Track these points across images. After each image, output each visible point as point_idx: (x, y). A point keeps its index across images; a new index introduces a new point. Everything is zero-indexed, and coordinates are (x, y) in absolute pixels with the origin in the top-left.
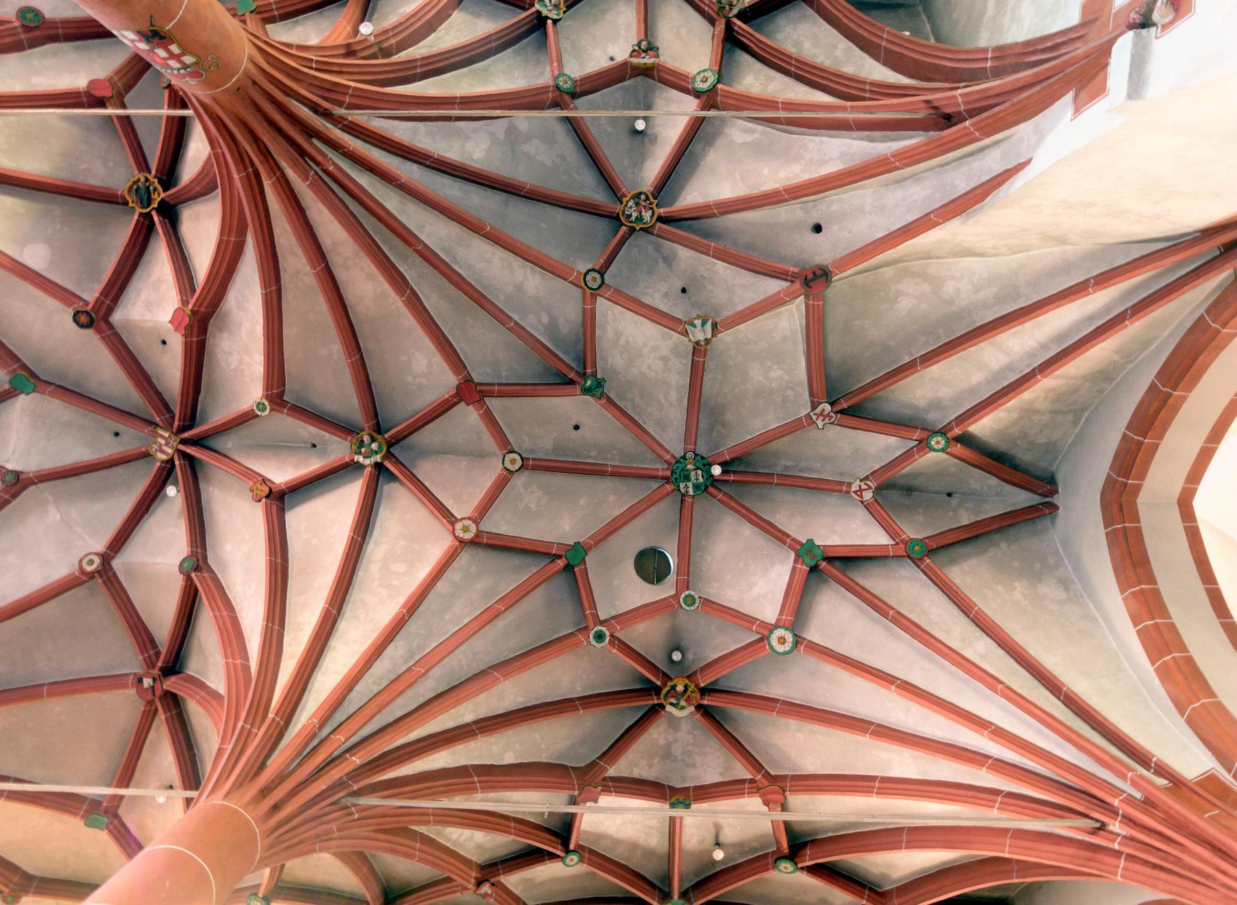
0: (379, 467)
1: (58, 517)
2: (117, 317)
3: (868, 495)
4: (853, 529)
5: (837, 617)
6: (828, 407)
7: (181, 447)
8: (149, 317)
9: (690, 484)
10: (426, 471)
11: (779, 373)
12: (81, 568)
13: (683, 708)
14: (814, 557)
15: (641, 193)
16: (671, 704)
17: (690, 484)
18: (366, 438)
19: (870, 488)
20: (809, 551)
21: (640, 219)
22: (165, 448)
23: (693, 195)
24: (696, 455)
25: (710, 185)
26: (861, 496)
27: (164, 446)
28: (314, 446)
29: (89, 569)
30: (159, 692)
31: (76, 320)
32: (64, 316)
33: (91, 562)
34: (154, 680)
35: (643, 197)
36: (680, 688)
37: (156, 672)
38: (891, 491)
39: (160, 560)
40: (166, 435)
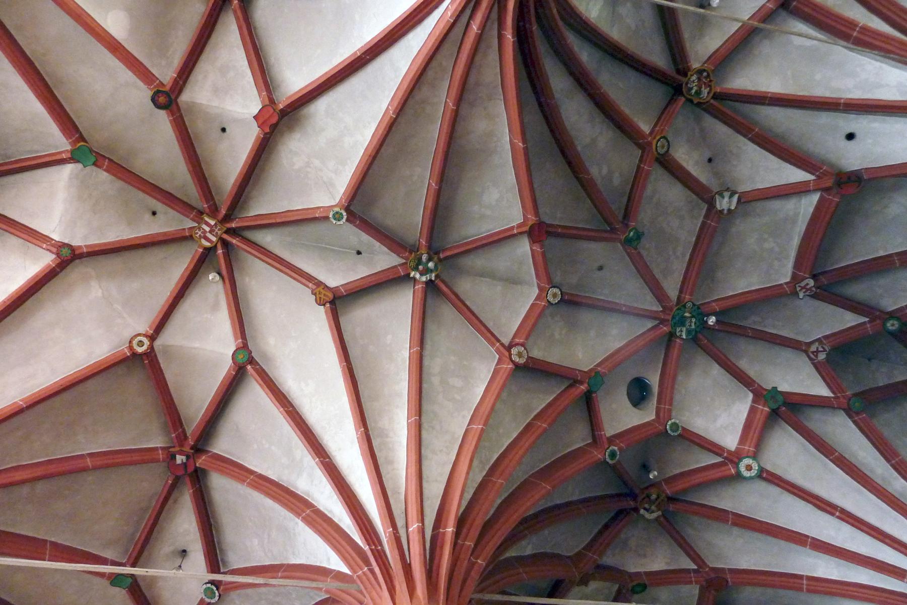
0: (430, 283)
1: (100, 293)
2: (185, 97)
3: (822, 356)
4: (800, 379)
5: (788, 452)
6: (811, 283)
7: (225, 236)
8: (215, 103)
9: (684, 329)
10: (465, 287)
11: (772, 245)
12: (131, 348)
13: (653, 512)
14: (776, 401)
15: (704, 70)
16: (645, 509)
17: (684, 329)
18: (424, 257)
19: (825, 350)
20: (772, 397)
21: (698, 93)
22: (209, 235)
23: (744, 80)
24: (694, 305)
25: (760, 75)
26: (816, 356)
27: (209, 232)
28: (359, 253)
29: (140, 350)
30: (191, 469)
31: (153, 100)
32: (142, 94)
33: (141, 344)
34: (188, 457)
35: (705, 74)
36: (654, 497)
37: (187, 449)
38: (837, 357)
39: (197, 345)
40: (212, 222)
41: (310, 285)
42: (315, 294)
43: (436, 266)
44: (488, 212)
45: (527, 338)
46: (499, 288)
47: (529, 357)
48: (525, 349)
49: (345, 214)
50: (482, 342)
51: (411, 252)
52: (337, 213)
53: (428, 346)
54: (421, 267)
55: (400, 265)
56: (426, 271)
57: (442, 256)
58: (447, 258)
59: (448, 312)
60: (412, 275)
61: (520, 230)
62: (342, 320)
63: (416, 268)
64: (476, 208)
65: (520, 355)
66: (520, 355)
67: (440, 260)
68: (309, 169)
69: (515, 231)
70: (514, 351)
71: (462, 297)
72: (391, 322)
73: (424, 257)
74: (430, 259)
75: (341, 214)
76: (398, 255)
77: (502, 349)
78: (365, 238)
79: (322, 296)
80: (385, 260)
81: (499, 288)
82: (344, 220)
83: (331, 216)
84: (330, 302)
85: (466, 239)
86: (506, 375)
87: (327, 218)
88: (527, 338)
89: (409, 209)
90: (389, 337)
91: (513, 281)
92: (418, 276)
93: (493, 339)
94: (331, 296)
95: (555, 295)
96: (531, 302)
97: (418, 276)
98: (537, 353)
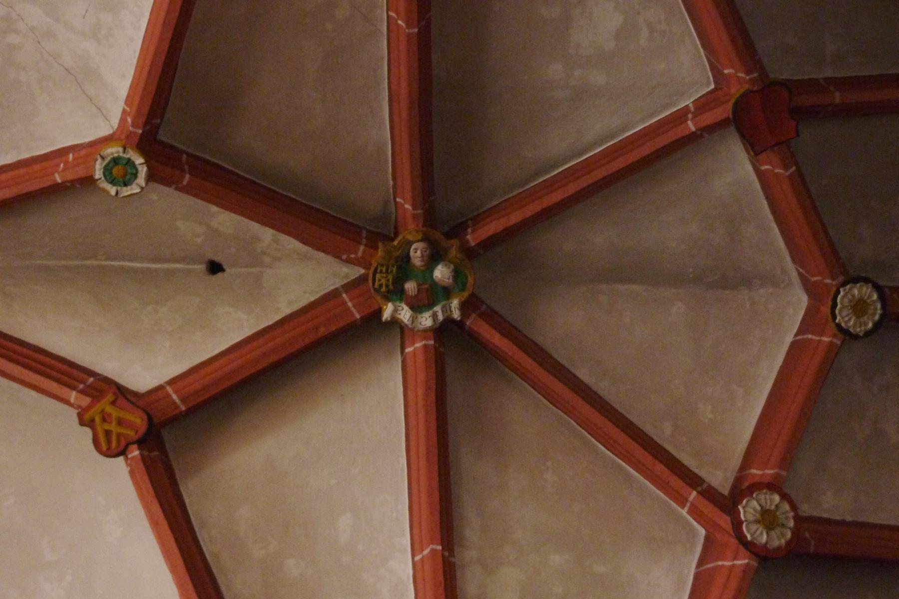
0: (445, 331)
10: (568, 322)
18: (417, 253)
28: (215, 268)
41: (73, 396)
42: (91, 424)
43: (457, 274)
44: (598, 78)
45: (787, 461)
46: (678, 308)
47: (798, 519)
48: (784, 497)
49: (139, 160)
50: (646, 494)
51: (372, 246)
52: (116, 161)
53: (471, 532)
54: (410, 286)
55: (349, 287)
56: (430, 296)
57: (472, 239)
58: (489, 244)
59: (524, 415)
60: (387, 314)
61: (709, 118)
62: (192, 491)
63: (396, 293)
64: (556, 70)
65: (768, 519)
66: (768, 519)
67: (470, 254)
68: (13, 39)
69: (691, 126)
70: (749, 509)
71: (561, 356)
72: (343, 470)
73: (417, 253)
74: (435, 257)
75: (129, 162)
76: (337, 256)
77: (708, 508)
78: (225, 220)
79: (113, 427)
80: (298, 278)
81: (678, 308)
82: (141, 180)
83: (98, 174)
84: (141, 443)
85: (538, 174)
86: (734, 584)
87: (88, 181)
88: (787, 461)
89: (347, 107)
90: (345, 521)
91: (722, 277)
92: (405, 314)
93: (676, 482)
94: (138, 420)
95: (859, 308)
96: (789, 339)
97: (405, 314)
98: (832, 503)
